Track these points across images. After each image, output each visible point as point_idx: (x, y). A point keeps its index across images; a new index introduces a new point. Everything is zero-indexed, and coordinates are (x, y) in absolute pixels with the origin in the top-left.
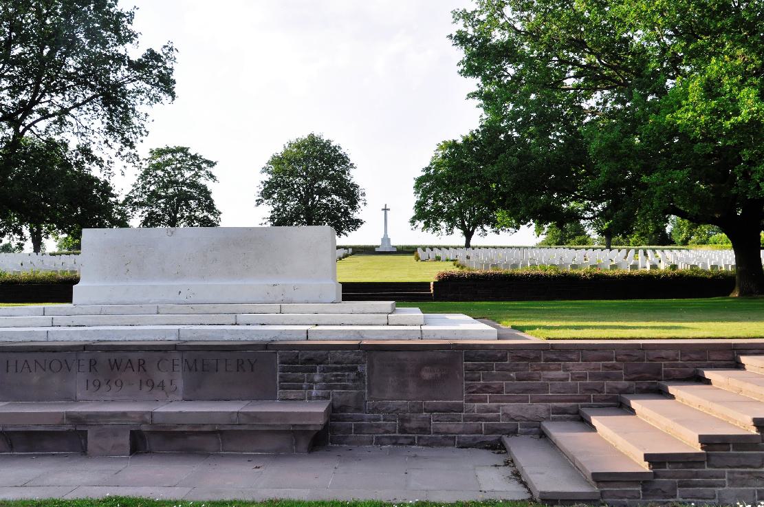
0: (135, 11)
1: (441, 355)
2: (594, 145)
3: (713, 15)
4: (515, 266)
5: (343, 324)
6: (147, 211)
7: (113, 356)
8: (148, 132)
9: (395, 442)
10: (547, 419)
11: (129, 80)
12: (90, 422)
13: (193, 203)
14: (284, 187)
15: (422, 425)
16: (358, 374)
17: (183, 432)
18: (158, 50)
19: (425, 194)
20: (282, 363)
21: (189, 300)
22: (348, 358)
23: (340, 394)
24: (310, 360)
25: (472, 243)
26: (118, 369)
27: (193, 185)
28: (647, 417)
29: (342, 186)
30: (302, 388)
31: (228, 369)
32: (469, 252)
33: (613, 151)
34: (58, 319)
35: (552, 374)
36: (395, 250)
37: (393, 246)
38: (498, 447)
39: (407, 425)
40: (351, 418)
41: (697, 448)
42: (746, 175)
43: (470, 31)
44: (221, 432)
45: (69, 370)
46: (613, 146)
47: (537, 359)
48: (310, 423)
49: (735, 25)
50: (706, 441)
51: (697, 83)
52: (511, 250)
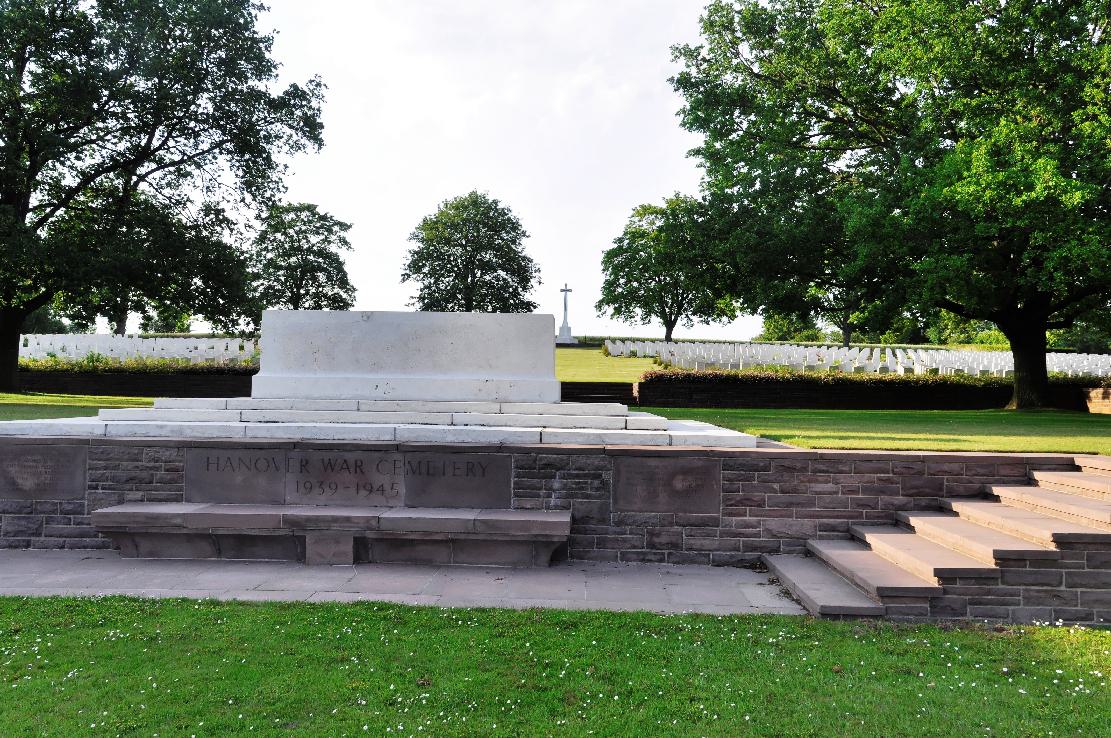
0: (275, 35)
1: (698, 463)
2: (851, 224)
3: (1003, 63)
4: (736, 366)
6: (262, 284)
8: (287, 188)
9: (643, 559)
10: (814, 537)
11: (266, 122)
13: (322, 277)
14: (438, 258)
15: (674, 539)
16: (602, 482)
18: (302, 85)
19: (617, 270)
20: (517, 467)
21: (387, 396)
24: (548, 465)
25: (674, 336)
26: (333, 470)
27: (321, 253)
28: (930, 534)
29: (513, 259)
30: (539, 496)
32: (671, 346)
33: (876, 230)
34: (247, 414)
35: (820, 487)
36: (576, 342)
37: (574, 337)
38: (759, 566)
39: (656, 540)
40: (594, 531)
41: (991, 564)
42: (1037, 263)
43: (694, 71)
46: (876, 223)
47: (804, 469)
48: (554, 533)
49: (1029, 77)
50: (1001, 557)
51: (983, 150)
52: (724, 346)
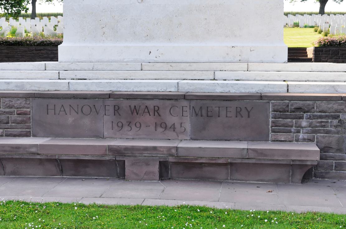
5: (308, 81)
7: (134, 103)
12: (128, 153)
16: (340, 121)
17: (201, 163)
20: (274, 111)
22: (332, 108)
23: (323, 137)
24: (299, 109)
25: (327, 9)
26: (137, 114)
30: (290, 132)
31: (228, 115)
40: (332, 158)
44: (231, 164)
45: (98, 114)
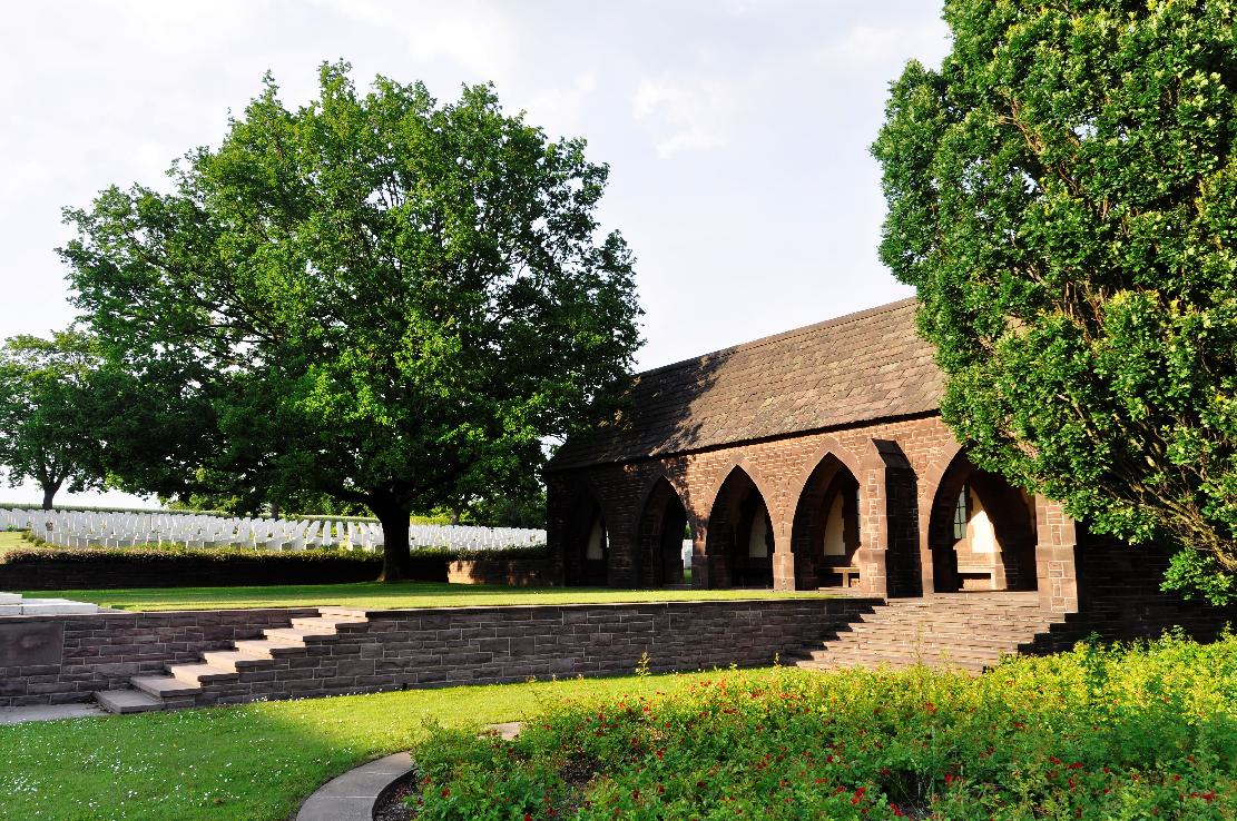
4: (126, 543)
15: (19, 687)
32: (50, 516)
38: (91, 700)
